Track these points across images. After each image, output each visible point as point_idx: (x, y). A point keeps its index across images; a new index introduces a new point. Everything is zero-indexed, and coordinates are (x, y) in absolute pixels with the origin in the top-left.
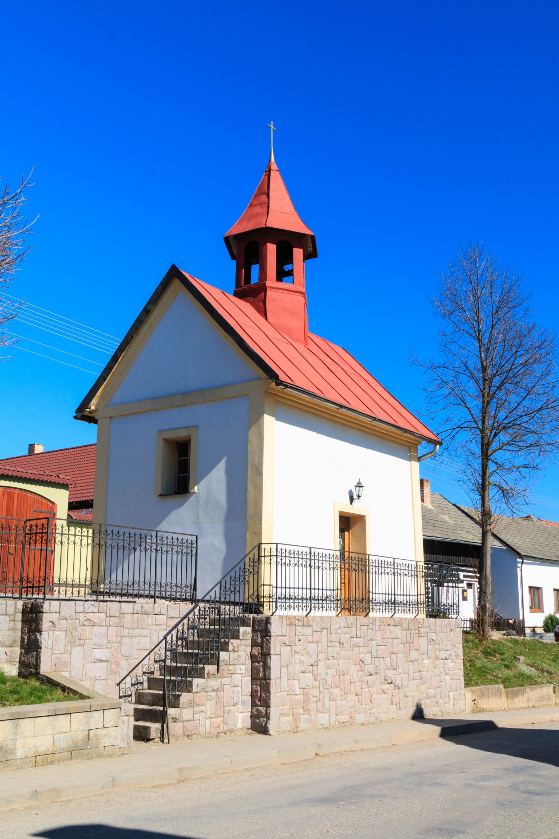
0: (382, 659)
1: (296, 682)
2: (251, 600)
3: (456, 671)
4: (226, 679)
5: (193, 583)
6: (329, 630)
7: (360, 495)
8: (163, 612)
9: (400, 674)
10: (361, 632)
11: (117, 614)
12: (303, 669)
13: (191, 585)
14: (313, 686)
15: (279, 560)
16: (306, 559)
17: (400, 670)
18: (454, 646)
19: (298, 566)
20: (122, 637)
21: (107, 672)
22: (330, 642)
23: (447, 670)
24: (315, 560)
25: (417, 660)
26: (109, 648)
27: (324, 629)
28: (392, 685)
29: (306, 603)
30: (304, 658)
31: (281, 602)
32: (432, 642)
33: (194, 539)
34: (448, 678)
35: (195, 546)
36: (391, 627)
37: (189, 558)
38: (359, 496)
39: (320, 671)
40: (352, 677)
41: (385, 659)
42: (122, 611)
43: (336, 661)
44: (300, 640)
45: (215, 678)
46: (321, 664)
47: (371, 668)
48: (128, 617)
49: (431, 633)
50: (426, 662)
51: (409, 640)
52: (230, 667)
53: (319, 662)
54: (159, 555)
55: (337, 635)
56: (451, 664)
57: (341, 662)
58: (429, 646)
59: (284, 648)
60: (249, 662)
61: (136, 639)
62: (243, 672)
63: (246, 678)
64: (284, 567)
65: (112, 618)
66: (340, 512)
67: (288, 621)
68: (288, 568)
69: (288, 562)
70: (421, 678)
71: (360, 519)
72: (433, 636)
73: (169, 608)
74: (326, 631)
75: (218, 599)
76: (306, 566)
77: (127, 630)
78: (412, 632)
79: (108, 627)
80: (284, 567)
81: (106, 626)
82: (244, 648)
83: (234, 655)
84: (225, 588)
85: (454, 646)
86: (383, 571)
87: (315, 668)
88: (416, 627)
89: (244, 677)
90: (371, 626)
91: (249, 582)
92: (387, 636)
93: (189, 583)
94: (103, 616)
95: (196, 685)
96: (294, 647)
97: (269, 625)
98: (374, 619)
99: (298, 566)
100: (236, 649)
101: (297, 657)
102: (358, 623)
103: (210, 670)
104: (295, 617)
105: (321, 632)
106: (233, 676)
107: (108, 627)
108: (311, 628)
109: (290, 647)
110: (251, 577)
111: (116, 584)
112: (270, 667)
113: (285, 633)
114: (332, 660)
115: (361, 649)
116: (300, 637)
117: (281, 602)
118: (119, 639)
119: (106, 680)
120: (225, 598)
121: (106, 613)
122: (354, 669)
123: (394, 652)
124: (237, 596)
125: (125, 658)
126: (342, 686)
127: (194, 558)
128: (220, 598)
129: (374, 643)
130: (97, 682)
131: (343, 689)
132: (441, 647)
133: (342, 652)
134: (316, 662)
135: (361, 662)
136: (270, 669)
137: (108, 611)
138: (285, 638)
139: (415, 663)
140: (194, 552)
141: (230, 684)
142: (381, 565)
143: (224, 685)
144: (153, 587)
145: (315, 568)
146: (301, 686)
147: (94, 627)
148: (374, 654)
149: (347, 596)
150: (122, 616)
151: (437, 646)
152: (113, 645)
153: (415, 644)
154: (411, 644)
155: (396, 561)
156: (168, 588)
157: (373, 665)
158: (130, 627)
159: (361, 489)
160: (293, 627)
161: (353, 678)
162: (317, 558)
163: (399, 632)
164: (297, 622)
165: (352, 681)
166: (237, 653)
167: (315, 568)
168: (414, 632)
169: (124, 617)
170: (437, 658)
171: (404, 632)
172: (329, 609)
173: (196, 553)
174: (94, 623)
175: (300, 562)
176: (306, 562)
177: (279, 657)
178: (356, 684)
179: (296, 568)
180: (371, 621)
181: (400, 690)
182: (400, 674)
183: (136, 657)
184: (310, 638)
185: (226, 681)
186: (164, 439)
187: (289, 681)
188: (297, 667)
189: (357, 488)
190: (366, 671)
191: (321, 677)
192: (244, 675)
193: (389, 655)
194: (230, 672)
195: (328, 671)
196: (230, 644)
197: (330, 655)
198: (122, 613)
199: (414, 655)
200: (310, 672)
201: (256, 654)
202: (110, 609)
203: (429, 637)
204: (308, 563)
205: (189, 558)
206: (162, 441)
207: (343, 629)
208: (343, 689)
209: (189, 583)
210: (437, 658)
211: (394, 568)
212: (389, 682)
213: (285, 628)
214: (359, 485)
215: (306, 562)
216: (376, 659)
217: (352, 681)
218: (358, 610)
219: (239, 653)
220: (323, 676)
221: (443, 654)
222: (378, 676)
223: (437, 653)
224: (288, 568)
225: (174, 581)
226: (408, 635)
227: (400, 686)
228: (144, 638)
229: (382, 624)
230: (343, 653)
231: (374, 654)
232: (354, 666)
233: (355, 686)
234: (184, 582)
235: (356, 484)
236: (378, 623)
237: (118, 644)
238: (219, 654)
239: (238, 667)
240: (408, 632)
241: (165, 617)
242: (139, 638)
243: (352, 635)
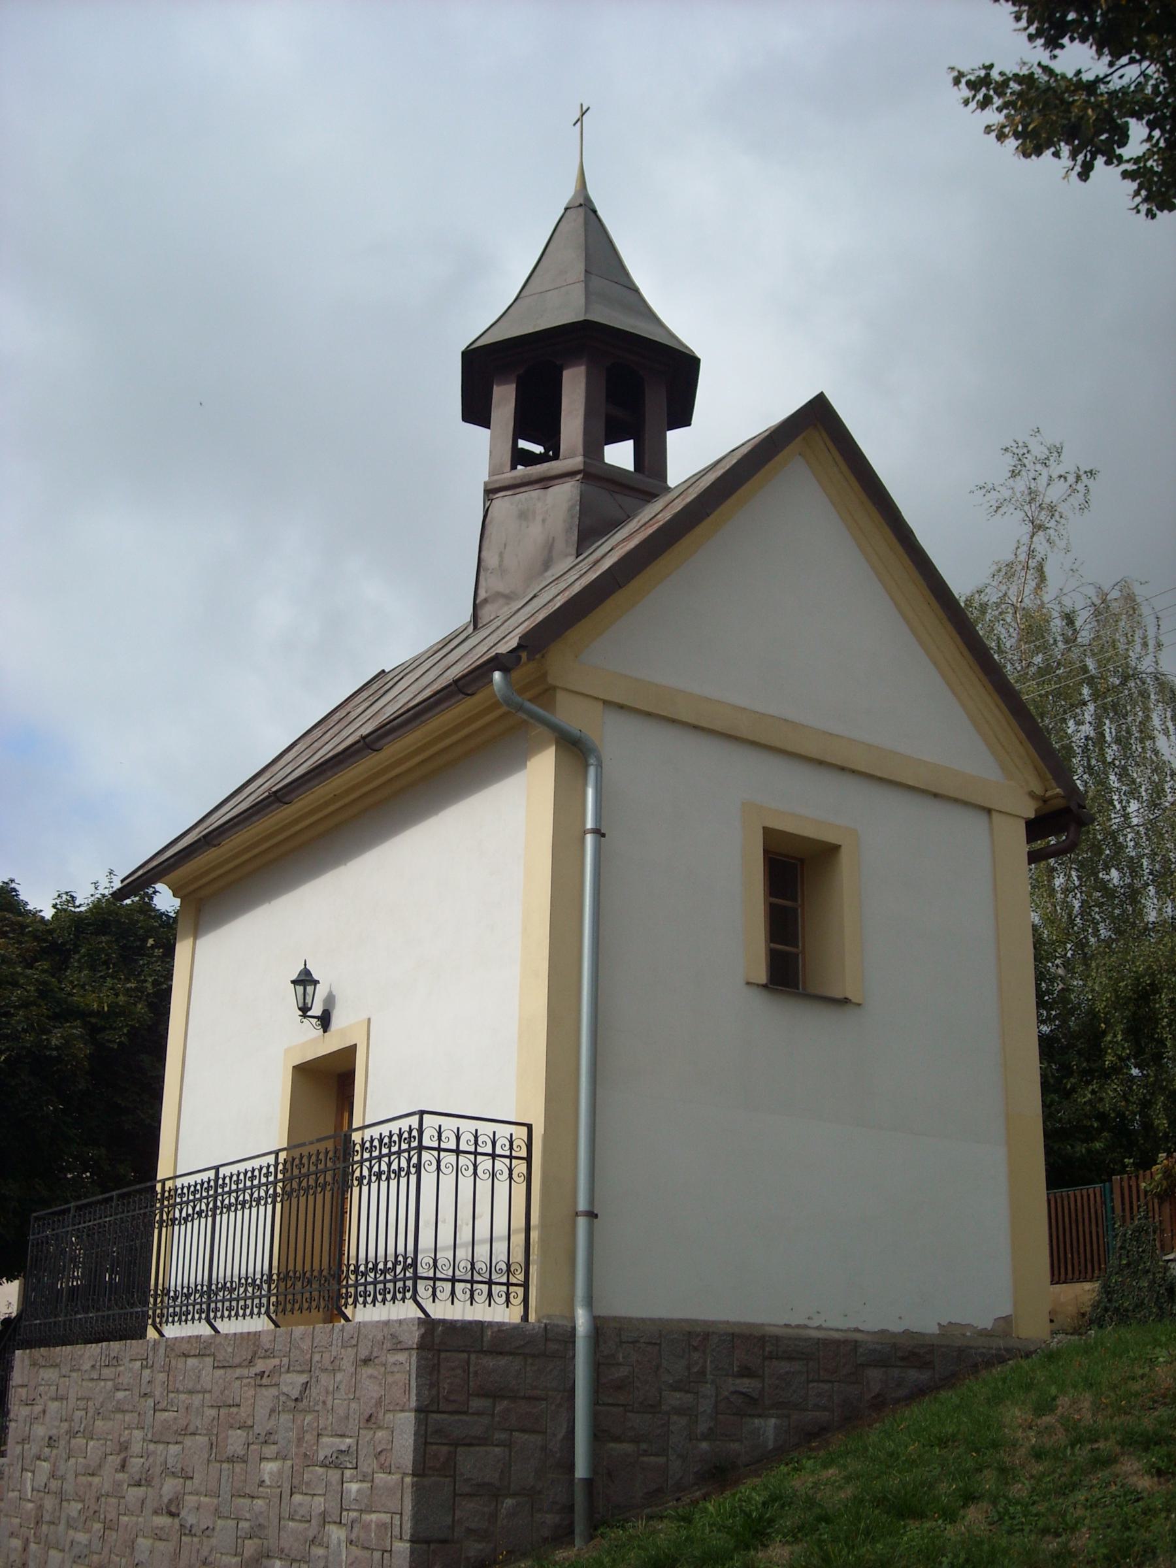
50: (270, 1467)
159: (310, 989)
170: (309, 1461)
189: (300, 989)
199: (235, 1441)
206: (831, 838)
210: (309, 1461)
235: (294, 977)
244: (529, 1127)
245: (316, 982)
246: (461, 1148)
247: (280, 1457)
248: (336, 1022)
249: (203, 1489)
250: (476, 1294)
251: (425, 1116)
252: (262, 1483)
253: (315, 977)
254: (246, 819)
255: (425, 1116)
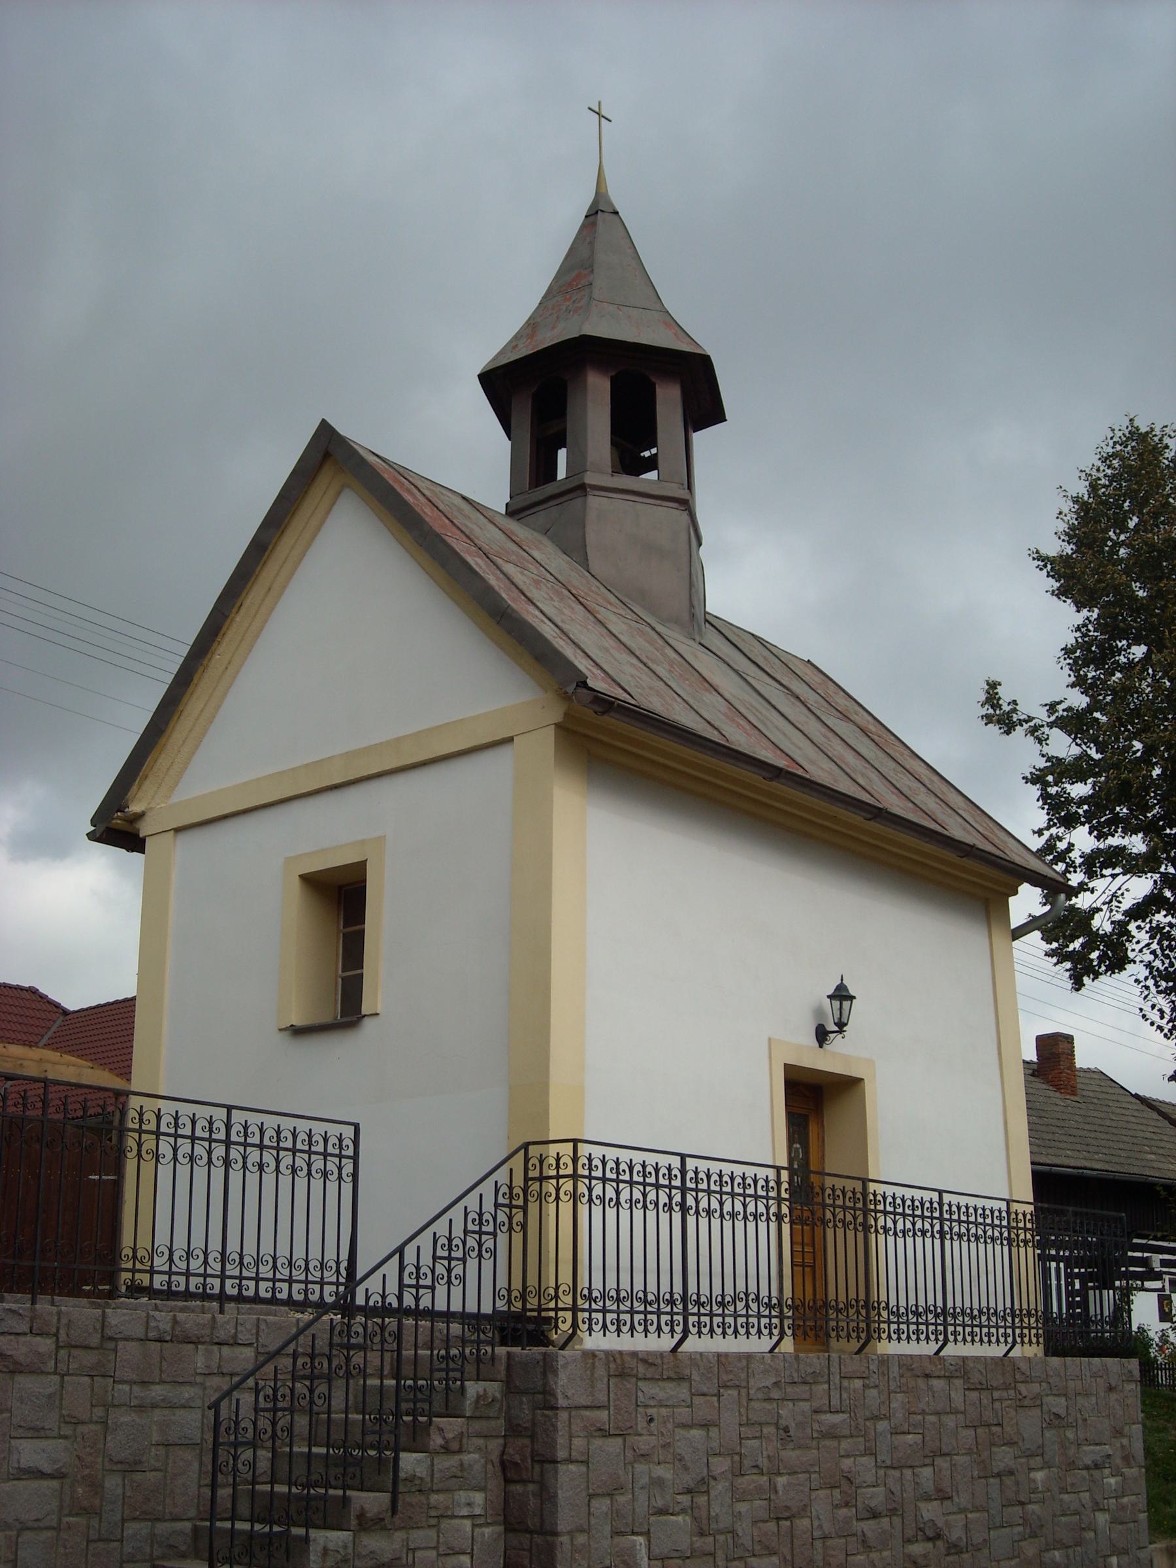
0: (908, 1473)
1: (640, 1539)
2: (501, 1305)
3: (1125, 1500)
4: (421, 1533)
5: (344, 1255)
6: (744, 1392)
7: (844, 1020)
8: (243, 1337)
9: (961, 1511)
10: (845, 1395)
11: (95, 1340)
12: (660, 1503)
13: (338, 1263)
14: (693, 1550)
15: (582, 1188)
16: (671, 1187)
17: (963, 1500)
18: (1118, 1433)
19: (645, 1207)
20: (107, 1406)
21: (61, 1507)
22: (749, 1424)
23: (1099, 1498)
24: (697, 1190)
25: (1011, 1473)
26: (66, 1437)
27: (726, 1387)
28: (939, 1543)
29: (672, 1314)
30: (660, 1471)
31: (699, 1315)
32: (1056, 1422)
33: (349, 1132)
34: (1102, 1518)
35: (350, 1152)
36: (935, 1382)
37: (332, 1187)
38: (841, 1025)
39: (715, 1510)
40: (816, 1523)
41: (917, 1470)
42: (109, 1332)
43: (765, 1478)
44: (651, 1420)
45: (384, 1528)
46: (719, 1488)
47: (876, 1497)
48: (129, 1351)
49: (1050, 1398)
50: (1039, 1476)
51: (988, 1415)
52: (434, 1498)
53: (712, 1483)
54: (235, 1176)
55: (768, 1406)
56: (1112, 1481)
57: (781, 1481)
58: (1047, 1434)
59: (598, 1442)
60: (495, 1484)
61: (157, 1415)
62: (478, 1511)
63: (487, 1531)
64: (597, 1211)
65: (74, 1352)
66: (787, 1067)
67: (612, 1366)
68: (611, 1213)
69: (610, 1193)
70: (1025, 1522)
71: (848, 1086)
72: (1058, 1405)
73: (263, 1326)
74: (734, 1393)
75: (393, 1300)
76: (671, 1209)
77: (126, 1388)
78: (996, 1395)
79: (62, 1376)
80: (597, 1211)
81: (55, 1373)
82: (481, 1441)
83: (447, 1464)
84: (418, 1268)
85: (1118, 1433)
86: (909, 1225)
87: (702, 1500)
88: (1010, 1380)
89: (480, 1526)
90: (874, 1379)
91: (494, 1254)
92: (922, 1406)
93: (330, 1255)
94: (45, 1345)
95: (319, 1548)
96: (629, 1439)
97: (550, 1376)
98: (885, 1360)
99: (645, 1207)
100: (455, 1446)
101: (640, 1467)
102: (835, 1369)
103: (367, 1507)
104: (634, 1354)
105: (719, 1395)
106: (445, 1524)
107: (62, 1376)
108: (686, 1384)
109: (620, 1440)
110: (502, 1238)
111: (241, 1263)
112: (556, 1496)
113: (602, 1398)
114: (755, 1477)
115: (845, 1445)
116: (652, 1411)
117: (590, 1310)
118: (99, 1412)
119: (57, 1529)
120: (417, 1299)
121: (56, 1335)
122: (821, 1503)
123: (945, 1449)
124: (456, 1292)
125: (119, 1467)
126: (786, 1550)
127: (347, 1188)
128: (400, 1298)
129: (882, 1426)
130: (27, 1536)
131: (789, 1557)
132: (1081, 1436)
133: (783, 1453)
134: (702, 1481)
135: (844, 1482)
136: (555, 1505)
137: (62, 1332)
138: (603, 1415)
139: (1008, 1481)
140: (348, 1168)
141: (436, 1548)
142: (900, 1209)
143: (414, 1550)
144: (218, 1266)
145: (697, 1213)
146: (656, 1551)
147: (19, 1378)
148: (884, 1457)
149: (774, 1293)
150: (111, 1345)
151: (1070, 1434)
152: (81, 1429)
153: (1007, 1429)
154: (994, 1429)
155: (947, 1198)
156: (851, 1312)
157: (882, 1489)
158: (135, 1377)
159: (846, 1004)
160: (629, 1384)
161: (820, 1527)
162: (703, 1186)
163: (957, 1398)
164: (642, 1369)
165: (816, 1534)
166: (457, 1457)
167: (697, 1213)
168: (1005, 1394)
169: (115, 1350)
170: (1072, 1465)
171: (973, 1395)
172: (742, 1331)
173: (355, 1175)
174: (16, 1363)
175: (652, 1196)
176: (670, 1198)
177: (583, 1469)
178: (829, 1542)
179: (638, 1214)
180: (873, 1367)
181: (965, 1556)
182: (961, 1511)
183: (158, 1465)
184: (683, 1413)
185: (418, 1537)
186: (303, 877)
187: (617, 1539)
188: (642, 1498)
189: (836, 1004)
190: (860, 1505)
191: (721, 1526)
192: (481, 1521)
193: (928, 1461)
194: (433, 1513)
195: (742, 1507)
196: (432, 1429)
197: (747, 1463)
198: (111, 1339)
199: (1004, 1457)
200: (683, 1511)
201: (517, 1459)
202: (68, 1326)
203: (1045, 1407)
204: (677, 1198)
205: (332, 1187)
206: (297, 882)
207: (789, 1389)
208: (789, 1557)
209: (330, 1255)
210: (1072, 1465)
211: (941, 1218)
212: (930, 1533)
213: (601, 1385)
214: (841, 995)
215: (670, 1198)
216: (891, 1472)
217: (816, 1534)
218: (811, 1333)
219: (466, 1458)
220: (725, 1521)
221: (1089, 1454)
222: (897, 1520)
223: (1072, 1451)
224: (611, 1213)
225: (283, 1251)
226: (985, 1402)
227: (963, 1544)
228: (180, 1413)
229: (909, 1374)
230: (790, 1455)
231: (884, 1457)
232: (822, 1493)
233: (825, 1547)
234: (315, 1253)
235: (831, 992)
236: (895, 1371)
237: (98, 1427)
238: (396, 1459)
239: (462, 1496)
240: (985, 1394)
241: (249, 1353)
242: (166, 1412)
243: (816, 1405)
244: (357, 1127)
245: (852, 998)
246: (197, 1135)
247: (1047, 1465)
248: (837, 1044)
249: (970, 1506)
250: (238, 1261)
251: (233, 1111)
252: (1035, 1491)
253: (852, 993)
254: (825, 794)
255: (233, 1111)
